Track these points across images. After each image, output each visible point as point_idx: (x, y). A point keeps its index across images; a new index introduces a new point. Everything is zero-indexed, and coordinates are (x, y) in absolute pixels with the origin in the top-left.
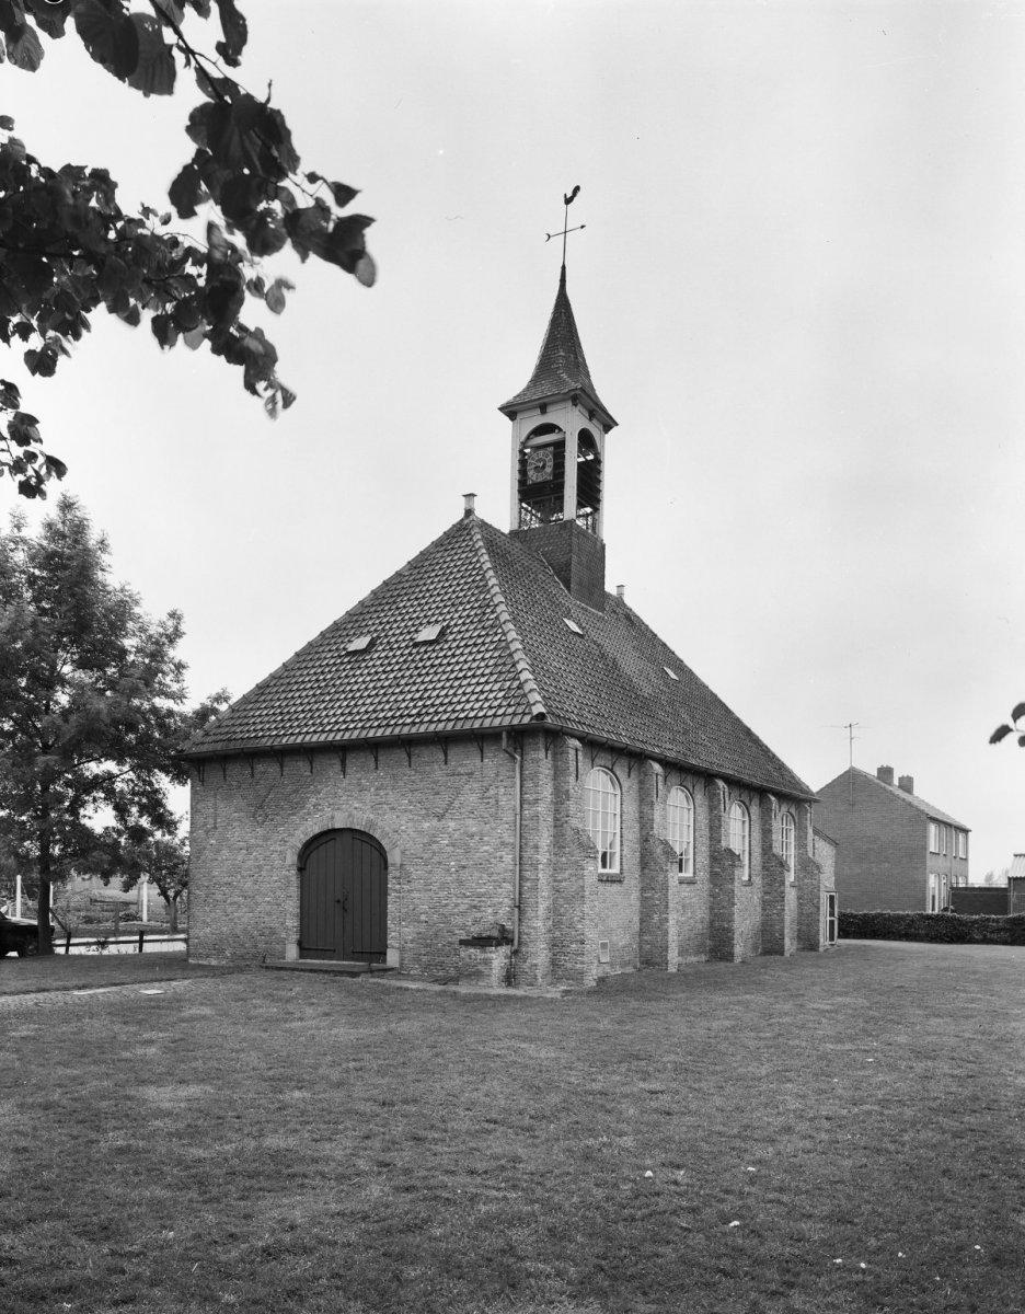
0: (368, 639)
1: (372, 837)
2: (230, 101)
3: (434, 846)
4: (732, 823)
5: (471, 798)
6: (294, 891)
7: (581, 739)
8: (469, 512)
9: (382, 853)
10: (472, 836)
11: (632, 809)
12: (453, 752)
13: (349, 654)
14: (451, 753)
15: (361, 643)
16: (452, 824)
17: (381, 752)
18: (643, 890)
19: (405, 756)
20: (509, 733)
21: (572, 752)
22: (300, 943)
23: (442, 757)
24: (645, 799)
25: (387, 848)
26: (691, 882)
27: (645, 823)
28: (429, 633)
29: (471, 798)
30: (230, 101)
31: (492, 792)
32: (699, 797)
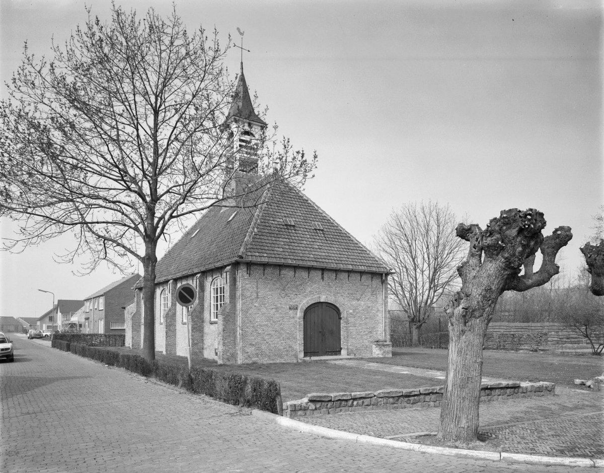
12: (364, 277)
16: (362, 302)
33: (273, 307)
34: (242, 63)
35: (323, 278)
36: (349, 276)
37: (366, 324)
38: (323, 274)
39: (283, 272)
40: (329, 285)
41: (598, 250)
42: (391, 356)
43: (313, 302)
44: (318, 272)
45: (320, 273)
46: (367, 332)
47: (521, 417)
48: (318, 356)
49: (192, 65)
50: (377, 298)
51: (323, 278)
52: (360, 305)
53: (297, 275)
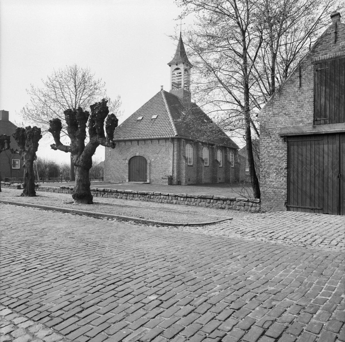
0: (142, 117)
1: (144, 158)
2: (125, 332)
3: (156, 159)
4: (218, 154)
5: (163, 150)
6: (128, 168)
7: (185, 139)
8: (162, 89)
9: (146, 161)
10: (164, 157)
11: (195, 152)
12: (160, 141)
13: (138, 120)
14: (341, 137)
15: (140, 118)
16: (160, 155)
17: (146, 141)
18: (197, 168)
19: (165, 141)
20: (171, 138)
21: (183, 142)
22: (129, 179)
23: (158, 142)
24: (226, 152)
25: (147, 160)
26: (208, 166)
27: (197, 154)
28: (154, 117)
29: (163, 150)
30: (125, 332)
31: (167, 149)
32: (223, 151)
33: (116, 159)
34: (181, 32)
35: (138, 144)
36: (152, 142)
37: (161, 166)
38: (138, 142)
39: (120, 143)
40: (141, 147)
41: (337, 63)
42: (167, 184)
43: (133, 156)
44: (156, 140)
45: (136, 142)
46: (162, 171)
47: (58, 223)
48: (136, 181)
49: (325, 5)
50: (169, 152)
51: (138, 144)
52: (158, 156)
53: (126, 144)
